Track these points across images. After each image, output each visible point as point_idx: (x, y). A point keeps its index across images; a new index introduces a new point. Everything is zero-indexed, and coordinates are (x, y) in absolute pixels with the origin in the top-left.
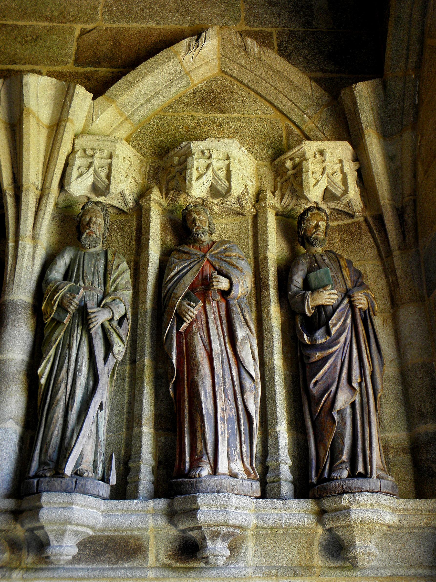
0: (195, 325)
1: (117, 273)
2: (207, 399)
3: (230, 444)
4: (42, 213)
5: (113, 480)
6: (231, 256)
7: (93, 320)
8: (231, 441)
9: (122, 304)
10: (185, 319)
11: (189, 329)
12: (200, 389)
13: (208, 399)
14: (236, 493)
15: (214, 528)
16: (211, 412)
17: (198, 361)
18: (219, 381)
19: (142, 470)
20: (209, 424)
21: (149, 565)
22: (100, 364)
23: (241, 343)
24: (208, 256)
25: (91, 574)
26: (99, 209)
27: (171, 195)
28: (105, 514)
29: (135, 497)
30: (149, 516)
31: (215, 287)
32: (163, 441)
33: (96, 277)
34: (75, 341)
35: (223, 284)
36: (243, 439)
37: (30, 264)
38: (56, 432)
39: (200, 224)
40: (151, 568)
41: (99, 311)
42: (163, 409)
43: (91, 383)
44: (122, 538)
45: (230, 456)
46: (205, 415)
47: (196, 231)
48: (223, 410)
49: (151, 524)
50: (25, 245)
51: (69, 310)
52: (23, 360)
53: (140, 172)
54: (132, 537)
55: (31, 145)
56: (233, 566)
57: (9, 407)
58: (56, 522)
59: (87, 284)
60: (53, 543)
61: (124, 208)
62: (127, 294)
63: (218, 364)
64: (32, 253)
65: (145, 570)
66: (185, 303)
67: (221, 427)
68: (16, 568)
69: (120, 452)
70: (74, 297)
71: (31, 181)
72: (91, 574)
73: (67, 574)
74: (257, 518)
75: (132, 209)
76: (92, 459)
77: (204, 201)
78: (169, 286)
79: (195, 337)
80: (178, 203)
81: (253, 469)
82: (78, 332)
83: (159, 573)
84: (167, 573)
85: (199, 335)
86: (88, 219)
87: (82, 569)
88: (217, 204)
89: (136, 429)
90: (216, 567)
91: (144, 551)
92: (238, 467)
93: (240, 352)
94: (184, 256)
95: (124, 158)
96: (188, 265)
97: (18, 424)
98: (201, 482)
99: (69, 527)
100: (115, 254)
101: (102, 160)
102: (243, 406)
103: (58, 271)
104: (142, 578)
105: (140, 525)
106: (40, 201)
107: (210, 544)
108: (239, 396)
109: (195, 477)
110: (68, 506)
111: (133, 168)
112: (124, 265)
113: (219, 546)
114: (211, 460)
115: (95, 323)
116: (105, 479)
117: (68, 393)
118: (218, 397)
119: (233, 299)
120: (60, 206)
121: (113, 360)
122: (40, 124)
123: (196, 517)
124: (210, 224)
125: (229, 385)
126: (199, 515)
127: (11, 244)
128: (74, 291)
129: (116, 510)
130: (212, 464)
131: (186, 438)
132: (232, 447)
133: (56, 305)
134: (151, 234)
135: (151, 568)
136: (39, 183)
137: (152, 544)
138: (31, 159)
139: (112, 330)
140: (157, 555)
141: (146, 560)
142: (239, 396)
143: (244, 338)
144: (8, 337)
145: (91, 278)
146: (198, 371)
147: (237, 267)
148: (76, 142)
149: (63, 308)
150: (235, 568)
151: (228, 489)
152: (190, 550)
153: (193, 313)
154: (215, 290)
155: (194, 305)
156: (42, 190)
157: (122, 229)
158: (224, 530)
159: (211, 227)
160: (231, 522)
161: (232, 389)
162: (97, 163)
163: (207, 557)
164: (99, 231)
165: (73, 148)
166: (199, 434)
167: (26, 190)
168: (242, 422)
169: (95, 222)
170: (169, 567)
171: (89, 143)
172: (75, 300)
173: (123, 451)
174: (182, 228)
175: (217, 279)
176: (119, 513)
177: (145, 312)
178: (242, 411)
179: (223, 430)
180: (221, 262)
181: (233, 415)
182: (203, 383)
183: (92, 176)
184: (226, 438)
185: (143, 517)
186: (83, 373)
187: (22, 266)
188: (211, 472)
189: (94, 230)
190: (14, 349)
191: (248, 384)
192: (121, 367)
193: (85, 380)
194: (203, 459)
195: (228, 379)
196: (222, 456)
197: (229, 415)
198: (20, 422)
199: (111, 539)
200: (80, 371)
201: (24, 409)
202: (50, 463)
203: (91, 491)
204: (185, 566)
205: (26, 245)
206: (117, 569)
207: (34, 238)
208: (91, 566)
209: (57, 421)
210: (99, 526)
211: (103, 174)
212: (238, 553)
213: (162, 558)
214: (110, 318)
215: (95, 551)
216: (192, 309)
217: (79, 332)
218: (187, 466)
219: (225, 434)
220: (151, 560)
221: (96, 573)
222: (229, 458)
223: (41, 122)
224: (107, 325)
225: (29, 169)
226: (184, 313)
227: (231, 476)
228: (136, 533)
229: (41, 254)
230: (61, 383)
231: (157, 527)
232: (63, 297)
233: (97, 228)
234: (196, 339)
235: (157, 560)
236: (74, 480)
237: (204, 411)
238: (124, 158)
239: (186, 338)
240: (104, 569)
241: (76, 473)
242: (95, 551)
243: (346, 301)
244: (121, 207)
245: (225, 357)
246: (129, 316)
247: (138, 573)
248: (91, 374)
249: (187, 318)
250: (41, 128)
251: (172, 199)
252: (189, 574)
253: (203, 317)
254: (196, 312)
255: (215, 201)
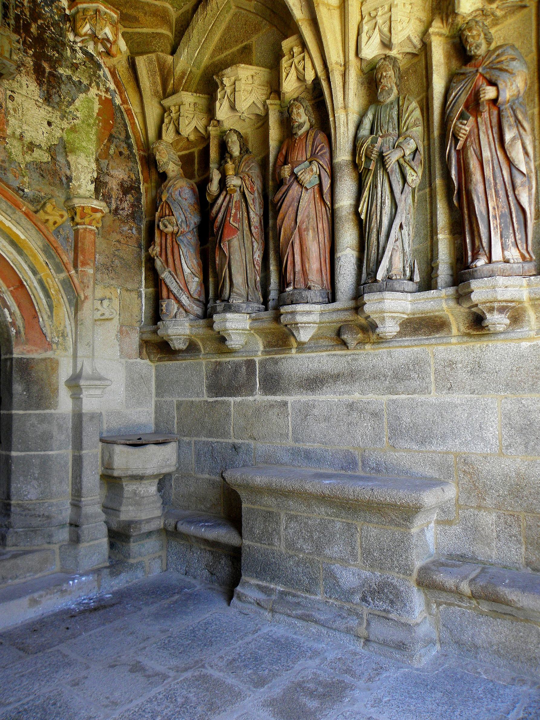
0: (469, 140)
1: (407, 115)
2: (479, 202)
3: (503, 236)
4: (347, 85)
5: (417, 278)
6: (502, 61)
7: (387, 161)
8: (504, 233)
9: (412, 140)
10: (459, 138)
11: (464, 147)
12: (473, 195)
13: (481, 202)
14: (507, 275)
15: (488, 305)
16: (484, 213)
17: (471, 172)
18: (490, 184)
19: (440, 268)
20: (483, 223)
21: (453, 335)
22: (398, 194)
23: (511, 145)
24: (480, 70)
25: (413, 343)
26: (387, 63)
27: (450, 20)
28: (412, 302)
29: (436, 288)
30: (443, 301)
31: (482, 99)
32: (459, 242)
33: (391, 124)
34: (379, 181)
35: (490, 93)
36: (516, 229)
37: (346, 129)
38: (373, 251)
39: (472, 40)
40: (454, 336)
41: (392, 152)
42: (457, 217)
43: (394, 210)
44: (430, 318)
45: (504, 246)
46: (478, 216)
47: (470, 49)
48: (494, 208)
49: (444, 306)
50: (339, 116)
51: (372, 158)
52: (351, 204)
53: (424, 10)
54: (436, 317)
55: (327, 31)
56: (519, 330)
57: (346, 240)
58: (376, 312)
59: (383, 132)
60: (380, 325)
61: (415, 51)
62: (418, 131)
63: (488, 169)
64: (346, 120)
65: (450, 338)
66: (458, 123)
67: (494, 223)
68: (367, 343)
69: (427, 257)
70: (374, 147)
71: (334, 62)
72: (413, 343)
73: (397, 344)
74: (530, 293)
75: (420, 49)
76: (401, 266)
77: (483, 11)
78: (448, 111)
79: (469, 151)
80: (457, 25)
81: (528, 253)
82: (380, 173)
83: (459, 339)
84: (465, 339)
85: (472, 149)
86: (380, 76)
87: (408, 340)
88: (497, 8)
89: (435, 237)
90: (496, 334)
91: (448, 325)
92: (513, 254)
93: (510, 152)
94: (462, 77)
95: (404, 4)
96: (464, 85)
97: (354, 250)
98: (476, 271)
99: (385, 314)
100: (405, 98)
101: (384, 16)
102: (515, 201)
103: (365, 128)
104: (448, 343)
105: (437, 308)
106: (344, 75)
107: (488, 316)
108: (510, 193)
109: (473, 268)
110: (381, 301)
111: (415, 9)
112: (414, 104)
113: (497, 317)
114: (487, 251)
115: (389, 163)
116: (411, 279)
117: (378, 222)
118: (489, 199)
119: (503, 105)
120: (366, 72)
121: (408, 188)
122: (331, 8)
123: (470, 298)
124: (485, 35)
125: (500, 186)
126: (472, 296)
127: (331, 119)
128: (374, 141)
129: (420, 299)
130: (488, 255)
131: (467, 238)
132: (505, 238)
133: (363, 157)
134: (434, 67)
135: (454, 336)
136: (341, 60)
137: (452, 319)
138: (329, 43)
139: (406, 165)
140: (458, 327)
141: (450, 331)
142: (510, 193)
143: (513, 139)
144: (338, 191)
145: (386, 126)
146: (471, 180)
147: (506, 71)
148: (362, 9)
149: (368, 158)
150: (520, 332)
151: (499, 273)
152: (477, 322)
153: (466, 131)
154: (483, 102)
155: (465, 122)
156: (345, 65)
157: (415, 72)
158: (496, 305)
159: (487, 37)
160: (499, 298)
161: (504, 189)
162: (380, 21)
163: (487, 326)
164: (390, 83)
165: (362, 15)
166: (476, 233)
167: (332, 71)
168: (514, 215)
169: (385, 76)
170: (468, 335)
171: (372, 4)
172: (375, 149)
173: (429, 255)
174: (460, 50)
175: (484, 91)
176: (423, 301)
177: (434, 139)
178: (514, 205)
179: (495, 225)
180: (492, 71)
181: (505, 211)
182: (476, 190)
183: (378, 35)
184: (499, 232)
185: (439, 301)
186: (387, 204)
187: (340, 133)
188: (487, 261)
189: (386, 84)
190: (344, 198)
191: (519, 180)
192: (421, 192)
193: (389, 209)
194: (480, 253)
195: (499, 181)
196: (495, 247)
197: (501, 212)
198: (355, 248)
199: (422, 319)
200: (384, 203)
201: (357, 239)
202: (372, 273)
203: (397, 289)
204: (480, 333)
205: (340, 115)
206: (430, 338)
207: (345, 107)
208: (413, 338)
209: (373, 244)
210: (409, 312)
211: (386, 30)
212: (523, 320)
213: (463, 329)
214: (402, 155)
215: (414, 328)
216: (463, 127)
217: (381, 173)
218: (470, 260)
219: (497, 228)
220: (454, 331)
221: (416, 342)
222: (503, 248)
223: (331, 6)
224: (402, 161)
225: (329, 53)
226: (457, 132)
227: (505, 262)
228: (437, 313)
229: (353, 118)
230: (373, 215)
231: (449, 308)
232: (367, 148)
233: (387, 82)
234: (469, 153)
235: (459, 330)
236: (385, 282)
237: (477, 213)
238: (404, 4)
239: (462, 154)
240: (421, 340)
241: (389, 278)
242: (414, 328)
243: (167, 206)
244: (412, 51)
245: (496, 162)
246: (421, 148)
247: (445, 340)
248: (393, 203)
249: (460, 137)
250: (333, 11)
251: (452, 24)
252: (482, 339)
253: (476, 130)
254: (468, 129)
255: (494, 6)
